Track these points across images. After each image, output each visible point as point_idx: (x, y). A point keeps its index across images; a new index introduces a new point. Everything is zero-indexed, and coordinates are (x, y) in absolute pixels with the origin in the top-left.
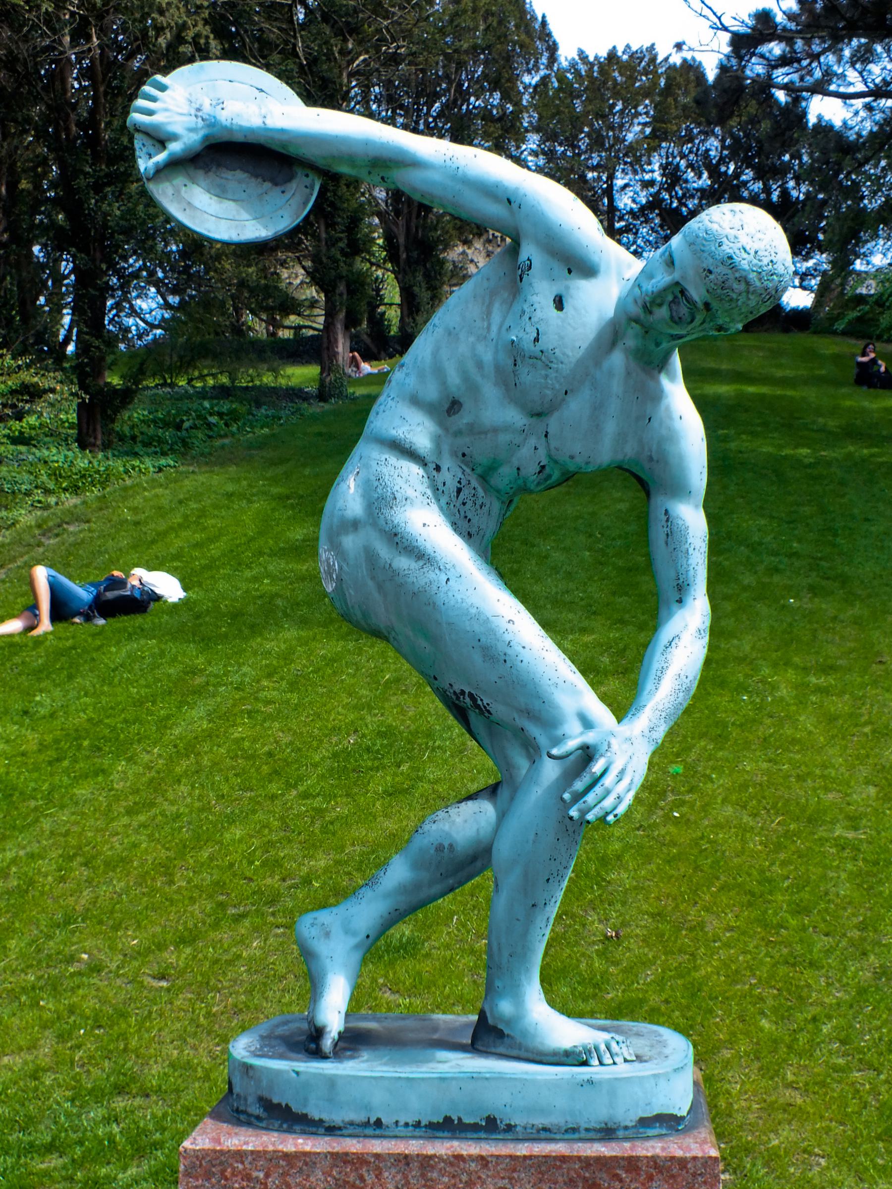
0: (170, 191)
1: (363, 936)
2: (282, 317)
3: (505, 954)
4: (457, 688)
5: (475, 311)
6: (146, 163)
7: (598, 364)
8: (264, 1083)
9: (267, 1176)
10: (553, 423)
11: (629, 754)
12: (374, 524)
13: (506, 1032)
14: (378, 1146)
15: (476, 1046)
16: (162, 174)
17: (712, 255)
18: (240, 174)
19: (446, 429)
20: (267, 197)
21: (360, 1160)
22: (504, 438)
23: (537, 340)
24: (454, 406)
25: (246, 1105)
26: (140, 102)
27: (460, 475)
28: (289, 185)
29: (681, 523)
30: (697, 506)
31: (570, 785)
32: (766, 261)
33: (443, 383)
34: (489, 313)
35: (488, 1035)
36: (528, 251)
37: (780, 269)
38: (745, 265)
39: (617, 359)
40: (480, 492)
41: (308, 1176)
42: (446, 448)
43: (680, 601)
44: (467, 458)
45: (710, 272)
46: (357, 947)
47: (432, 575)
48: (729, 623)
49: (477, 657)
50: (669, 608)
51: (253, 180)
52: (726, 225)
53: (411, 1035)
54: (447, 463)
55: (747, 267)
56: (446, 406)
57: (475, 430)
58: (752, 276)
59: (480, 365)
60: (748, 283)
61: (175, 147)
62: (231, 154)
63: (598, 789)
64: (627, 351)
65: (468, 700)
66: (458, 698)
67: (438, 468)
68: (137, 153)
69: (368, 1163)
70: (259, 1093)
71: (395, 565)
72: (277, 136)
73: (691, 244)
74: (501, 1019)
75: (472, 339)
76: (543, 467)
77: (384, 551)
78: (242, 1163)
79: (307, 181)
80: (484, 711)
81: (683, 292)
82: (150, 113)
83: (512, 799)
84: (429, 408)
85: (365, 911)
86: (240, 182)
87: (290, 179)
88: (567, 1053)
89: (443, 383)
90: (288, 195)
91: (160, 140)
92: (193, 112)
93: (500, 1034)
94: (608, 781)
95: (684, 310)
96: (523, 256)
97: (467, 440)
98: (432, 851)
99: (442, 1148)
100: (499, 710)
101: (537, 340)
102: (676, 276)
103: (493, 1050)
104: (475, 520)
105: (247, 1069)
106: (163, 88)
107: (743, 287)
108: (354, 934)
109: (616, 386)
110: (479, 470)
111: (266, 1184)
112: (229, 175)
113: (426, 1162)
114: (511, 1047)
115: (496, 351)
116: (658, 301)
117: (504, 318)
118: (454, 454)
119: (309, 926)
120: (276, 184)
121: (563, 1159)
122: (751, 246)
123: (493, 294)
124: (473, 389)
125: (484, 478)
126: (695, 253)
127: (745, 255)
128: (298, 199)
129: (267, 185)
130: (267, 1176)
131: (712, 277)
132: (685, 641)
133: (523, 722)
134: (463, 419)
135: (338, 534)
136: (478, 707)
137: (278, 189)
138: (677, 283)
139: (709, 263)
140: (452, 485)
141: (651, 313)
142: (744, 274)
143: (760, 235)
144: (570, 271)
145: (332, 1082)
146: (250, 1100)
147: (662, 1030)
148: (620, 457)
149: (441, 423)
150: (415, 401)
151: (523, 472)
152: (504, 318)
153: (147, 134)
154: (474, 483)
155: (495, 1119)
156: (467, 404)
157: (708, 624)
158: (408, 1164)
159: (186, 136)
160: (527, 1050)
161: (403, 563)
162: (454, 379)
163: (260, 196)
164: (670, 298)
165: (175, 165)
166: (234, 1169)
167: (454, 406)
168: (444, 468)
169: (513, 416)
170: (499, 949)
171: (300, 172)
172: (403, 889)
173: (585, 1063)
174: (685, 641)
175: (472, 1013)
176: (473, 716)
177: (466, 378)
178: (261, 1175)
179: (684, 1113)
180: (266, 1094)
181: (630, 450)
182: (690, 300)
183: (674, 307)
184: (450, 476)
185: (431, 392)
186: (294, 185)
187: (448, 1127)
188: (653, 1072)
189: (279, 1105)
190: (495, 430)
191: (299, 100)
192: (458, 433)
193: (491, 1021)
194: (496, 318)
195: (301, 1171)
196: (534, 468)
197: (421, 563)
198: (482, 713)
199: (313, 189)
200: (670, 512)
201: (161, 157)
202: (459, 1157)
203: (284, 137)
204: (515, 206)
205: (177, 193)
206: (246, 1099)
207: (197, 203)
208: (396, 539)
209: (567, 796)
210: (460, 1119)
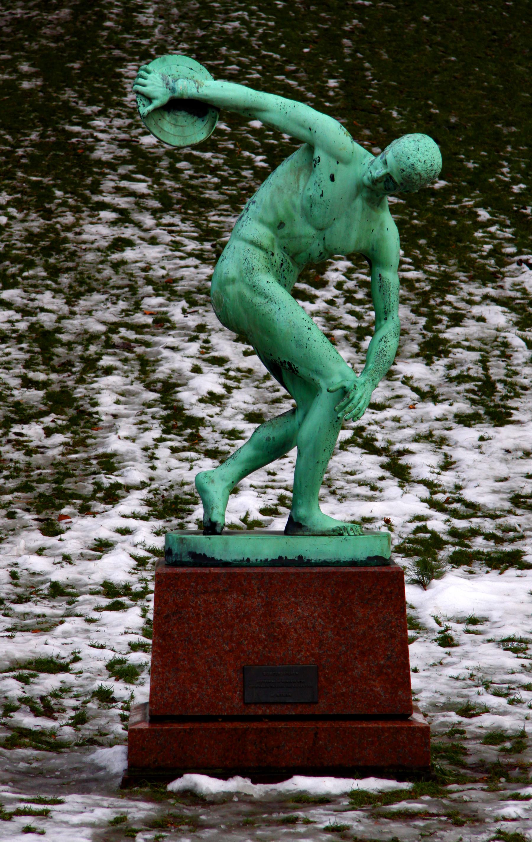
1: (231, 482)
2: (412, 306)
3: (304, 487)
4: (282, 360)
5: (291, 178)
7: (349, 205)
9: (197, 585)
10: (327, 233)
12: (243, 281)
13: (303, 524)
14: (249, 570)
17: (405, 163)
18: (184, 113)
19: (277, 235)
20: (196, 124)
23: (322, 195)
24: (281, 225)
32: (429, 165)
33: (276, 214)
34: (298, 180)
36: (318, 153)
38: (419, 168)
39: (359, 203)
42: (276, 244)
43: (386, 319)
46: (228, 487)
47: (272, 306)
49: (293, 345)
52: (411, 149)
54: (277, 251)
56: (277, 224)
57: (291, 237)
58: (423, 173)
59: (294, 206)
60: (420, 176)
61: (156, 103)
62: (182, 105)
64: (363, 199)
67: (273, 254)
71: (254, 301)
73: (396, 157)
74: (300, 518)
75: (290, 192)
77: (248, 294)
79: (214, 114)
80: (293, 371)
81: (391, 177)
82: (144, 86)
83: (305, 416)
84: (269, 225)
86: (184, 116)
88: (334, 530)
89: (276, 214)
90: (205, 122)
91: (150, 99)
95: (391, 185)
96: (316, 155)
97: (287, 241)
100: (302, 371)
101: (322, 195)
102: (388, 170)
106: (148, 72)
107: (418, 177)
108: (226, 481)
112: (178, 113)
113: (271, 575)
115: (302, 200)
117: (306, 184)
118: (280, 247)
121: (334, 573)
122: (423, 158)
123: (300, 170)
124: (291, 218)
126: (397, 161)
128: (208, 125)
129: (196, 118)
134: (285, 231)
135: (225, 285)
136: (292, 369)
137: (200, 120)
138: (388, 174)
139: (403, 166)
140: (279, 262)
146: (183, 555)
148: (358, 248)
149: (274, 233)
150: (262, 221)
152: (306, 184)
154: (289, 261)
156: (287, 224)
159: (161, 95)
161: (258, 300)
162: (281, 212)
164: (385, 179)
167: (281, 225)
169: (310, 231)
171: (210, 111)
177: (286, 210)
180: (193, 550)
181: (363, 245)
182: (394, 181)
185: (270, 218)
186: (208, 117)
188: (491, 180)
190: (300, 237)
192: (283, 237)
193: (295, 520)
194: (302, 182)
196: (317, 254)
201: (150, 108)
202: (287, 574)
204: (313, 131)
206: (181, 555)
207: (166, 129)
209: (337, 408)
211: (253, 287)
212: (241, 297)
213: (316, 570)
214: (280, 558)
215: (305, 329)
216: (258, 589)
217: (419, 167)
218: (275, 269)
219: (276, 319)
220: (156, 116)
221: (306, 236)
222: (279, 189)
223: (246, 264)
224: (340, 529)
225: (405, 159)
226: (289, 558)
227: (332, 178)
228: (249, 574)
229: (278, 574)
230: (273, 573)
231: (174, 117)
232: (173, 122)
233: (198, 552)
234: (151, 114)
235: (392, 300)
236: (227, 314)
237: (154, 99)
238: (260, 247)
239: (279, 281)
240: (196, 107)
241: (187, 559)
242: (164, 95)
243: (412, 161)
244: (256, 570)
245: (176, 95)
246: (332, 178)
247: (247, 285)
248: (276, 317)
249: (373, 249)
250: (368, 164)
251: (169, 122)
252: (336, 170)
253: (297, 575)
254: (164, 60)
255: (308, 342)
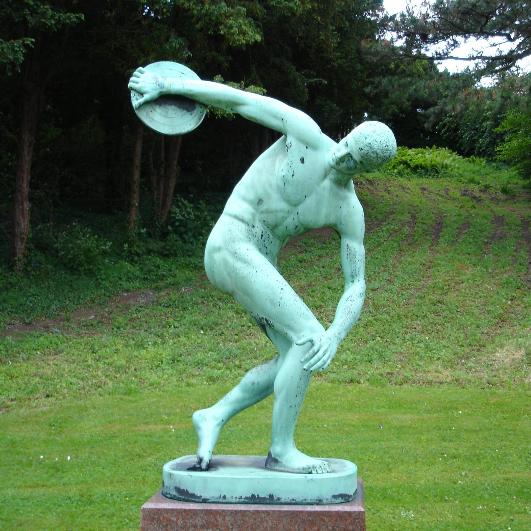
0: (145, 114)
4: (260, 316)
6: (136, 101)
7: (318, 184)
8: (177, 481)
9: (177, 519)
10: (300, 209)
11: (329, 343)
12: (227, 249)
15: (268, 466)
16: (142, 107)
18: (173, 107)
19: (257, 211)
20: (184, 116)
21: (217, 512)
22: (280, 215)
23: (293, 175)
24: (260, 201)
25: (170, 490)
26: (132, 79)
27: (263, 229)
28: (193, 111)
29: (353, 249)
30: (360, 243)
31: (304, 355)
34: (274, 164)
35: (271, 462)
37: (390, 148)
38: (376, 147)
39: (327, 183)
40: (271, 236)
41: (195, 519)
43: (353, 282)
44: (265, 222)
45: (362, 149)
46: (218, 425)
48: (383, 297)
50: (348, 285)
51: (179, 109)
53: (240, 463)
54: (257, 224)
55: (376, 148)
56: (257, 201)
58: (379, 151)
61: (147, 97)
63: (316, 358)
65: (265, 322)
66: (261, 321)
67: (253, 227)
68: (132, 98)
69: (219, 513)
70: (175, 485)
71: (235, 266)
72: (188, 92)
76: (297, 226)
77: (231, 260)
78: (167, 514)
80: (271, 326)
81: (351, 157)
84: (251, 203)
85: (221, 409)
86: (173, 110)
87: (194, 109)
90: (193, 116)
92: (155, 83)
93: (276, 461)
94: (320, 354)
96: (288, 142)
98: (250, 385)
99: (253, 508)
100: (277, 325)
101: (293, 175)
103: (274, 468)
104: (269, 248)
105: (171, 475)
109: (326, 194)
110: (270, 227)
111: (177, 523)
112: (169, 107)
113: (244, 513)
114: (281, 466)
116: (342, 160)
118: (260, 221)
119: (197, 415)
120: (188, 111)
122: (379, 139)
125: (272, 231)
127: (376, 143)
130: (177, 519)
131: (362, 151)
132: (353, 297)
133: (286, 330)
134: (264, 207)
136: (269, 324)
137: (189, 113)
138: (349, 154)
139: (361, 146)
140: (259, 233)
141: (339, 165)
142: (375, 150)
143: (382, 135)
144: (307, 148)
145: (205, 479)
146: (171, 488)
147: (343, 460)
150: (244, 199)
151: (288, 228)
153: (135, 90)
154: (269, 233)
155: (273, 495)
157: (364, 290)
158: (236, 514)
159: (151, 93)
160: (287, 468)
161: (238, 265)
163: (182, 116)
165: (147, 103)
166: (164, 517)
168: (256, 226)
170: (277, 425)
172: (237, 401)
173: (311, 473)
174: (353, 297)
175: (265, 455)
176: (268, 329)
178: (175, 519)
179: (352, 493)
180: (178, 486)
181: (332, 220)
183: (348, 163)
184: (259, 229)
185: (251, 196)
186: (195, 111)
187: (254, 499)
189: (183, 490)
191: (198, 77)
192: (262, 213)
193: (273, 456)
195: (191, 517)
197: (246, 265)
198: (270, 327)
199: (203, 113)
200: (349, 245)
201: (142, 100)
203: (192, 93)
205: (147, 115)
208: (236, 255)
210: (258, 495)
211: (235, 254)
212: (226, 263)
213: (286, 508)
214: (253, 496)
215: (279, 290)
216: (232, 525)
217: (376, 147)
218: (256, 239)
219: (253, 281)
220: (148, 109)
221: (281, 211)
222: (263, 173)
223: (229, 235)
224: (310, 468)
225: (363, 139)
226: (261, 496)
227: (302, 161)
228: (223, 511)
229: (249, 511)
230: (246, 511)
231: (165, 110)
232: (164, 114)
233: (182, 488)
234: (141, 106)
235: (358, 266)
236: (215, 280)
237: (145, 93)
238: (242, 220)
239: (260, 250)
240: (183, 101)
241: (174, 493)
242: (154, 90)
243: (369, 140)
244: (230, 507)
245: (164, 90)
246: (302, 161)
247: (230, 252)
248: (253, 280)
249: (341, 223)
250: (332, 150)
251: (161, 114)
252: (306, 155)
253: (267, 513)
254: (159, 65)
255: (281, 301)
